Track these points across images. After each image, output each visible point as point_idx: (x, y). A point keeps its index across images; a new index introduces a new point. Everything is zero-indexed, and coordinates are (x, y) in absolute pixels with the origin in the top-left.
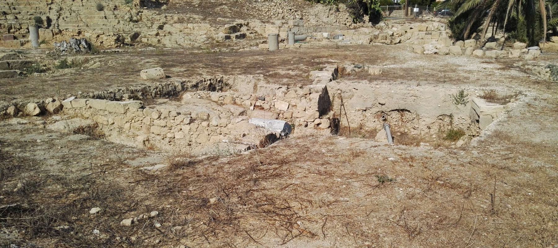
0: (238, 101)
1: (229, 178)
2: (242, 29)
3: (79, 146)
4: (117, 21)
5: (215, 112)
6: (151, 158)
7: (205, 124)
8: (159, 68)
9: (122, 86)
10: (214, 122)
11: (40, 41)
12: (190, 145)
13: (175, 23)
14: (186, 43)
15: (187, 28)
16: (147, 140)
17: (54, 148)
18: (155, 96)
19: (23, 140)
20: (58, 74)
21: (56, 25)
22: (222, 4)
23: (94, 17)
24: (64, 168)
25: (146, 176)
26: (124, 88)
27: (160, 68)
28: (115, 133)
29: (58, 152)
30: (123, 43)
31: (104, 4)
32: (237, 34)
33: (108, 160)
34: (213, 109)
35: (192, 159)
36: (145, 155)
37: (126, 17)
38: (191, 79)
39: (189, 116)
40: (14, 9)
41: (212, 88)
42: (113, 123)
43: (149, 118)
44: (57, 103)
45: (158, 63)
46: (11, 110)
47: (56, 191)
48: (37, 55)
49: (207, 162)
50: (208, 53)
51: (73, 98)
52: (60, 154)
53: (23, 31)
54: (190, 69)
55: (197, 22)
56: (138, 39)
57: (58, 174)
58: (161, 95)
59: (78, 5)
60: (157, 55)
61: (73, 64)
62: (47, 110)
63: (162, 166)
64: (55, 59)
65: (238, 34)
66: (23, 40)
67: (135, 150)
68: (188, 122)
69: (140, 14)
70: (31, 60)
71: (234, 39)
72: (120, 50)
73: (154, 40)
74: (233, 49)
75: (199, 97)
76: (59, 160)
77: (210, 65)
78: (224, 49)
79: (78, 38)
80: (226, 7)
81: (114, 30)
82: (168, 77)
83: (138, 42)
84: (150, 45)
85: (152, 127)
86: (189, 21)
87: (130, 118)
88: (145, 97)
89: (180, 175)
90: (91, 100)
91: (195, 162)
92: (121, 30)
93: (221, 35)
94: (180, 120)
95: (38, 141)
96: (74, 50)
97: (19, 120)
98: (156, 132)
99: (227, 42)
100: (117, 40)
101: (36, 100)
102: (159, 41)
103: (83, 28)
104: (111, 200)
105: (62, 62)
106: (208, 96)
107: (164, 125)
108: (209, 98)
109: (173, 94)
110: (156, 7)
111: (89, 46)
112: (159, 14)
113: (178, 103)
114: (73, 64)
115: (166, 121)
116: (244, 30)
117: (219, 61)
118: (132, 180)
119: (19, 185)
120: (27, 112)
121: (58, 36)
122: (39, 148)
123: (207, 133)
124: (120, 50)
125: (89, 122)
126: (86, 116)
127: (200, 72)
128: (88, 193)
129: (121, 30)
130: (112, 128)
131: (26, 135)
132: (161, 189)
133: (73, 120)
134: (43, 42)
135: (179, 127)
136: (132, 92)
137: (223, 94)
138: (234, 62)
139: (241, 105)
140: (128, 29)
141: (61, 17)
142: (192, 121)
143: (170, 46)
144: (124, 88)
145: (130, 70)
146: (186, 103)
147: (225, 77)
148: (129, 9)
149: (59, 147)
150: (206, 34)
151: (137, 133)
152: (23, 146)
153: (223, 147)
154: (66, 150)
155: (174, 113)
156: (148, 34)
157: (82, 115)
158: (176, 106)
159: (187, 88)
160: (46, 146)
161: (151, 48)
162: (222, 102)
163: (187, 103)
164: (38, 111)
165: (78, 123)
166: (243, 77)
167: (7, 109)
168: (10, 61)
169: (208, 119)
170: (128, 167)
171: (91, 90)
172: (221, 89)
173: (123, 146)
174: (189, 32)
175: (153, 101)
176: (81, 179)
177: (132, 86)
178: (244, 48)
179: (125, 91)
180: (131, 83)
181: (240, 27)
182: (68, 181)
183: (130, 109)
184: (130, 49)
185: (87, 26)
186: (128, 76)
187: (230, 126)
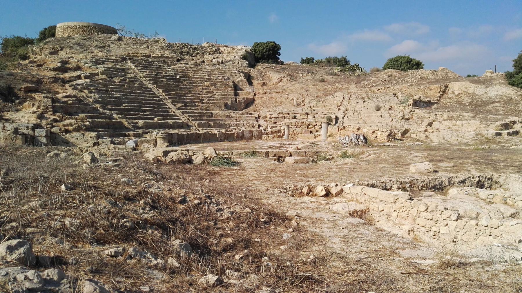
0: (509, 201)
1: (506, 288)
2: (515, 126)
3: (357, 229)
4: (391, 119)
5: (483, 210)
6: (421, 252)
7: (473, 222)
8: (427, 163)
9: (393, 178)
10: (484, 222)
11: (328, 135)
12: (455, 242)
13: (445, 120)
14: (453, 139)
15: (456, 125)
16: (412, 231)
17: (337, 228)
18: (422, 189)
19: (314, 217)
20: (341, 163)
21: (342, 122)
22: (494, 102)
23: (372, 116)
24: (345, 247)
25: (417, 269)
26: (394, 180)
27: (429, 163)
28: (383, 220)
29: (340, 232)
30: (394, 138)
31: (381, 105)
32: (509, 131)
33: (381, 247)
34: (481, 207)
35: (463, 260)
36: (415, 248)
37: (400, 115)
38: (458, 175)
39: (456, 212)
40: (314, 110)
41: (480, 185)
42: (382, 211)
43: (416, 209)
44: (339, 188)
45: (426, 157)
46: (305, 190)
47: (339, 268)
48: (325, 146)
49: (479, 266)
50: (476, 149)
51: (352, 184)
52: (342, 234)
53: (317, 127)
54: (458, 164)
55: (466, 120)
56: (408, 135)
57: (340, 252)
58: (427, 188)
59: (360, 106)
60: (425, 150)
61: (352, 155)
62: (330, 193)
63: (432, 261)
64: (338, 150)
65: (511, 131)
66: (316, 134)
67: (405, 240)
68: (455, 218)
69: (412, 113)
70: (321, 150)
71: (506, 136)
72: (391, 144)
73: (422, 136)
74: (504, 146)
75: (466, 193)
76: (341, 239)
77: (479, 162)
78: (494, 146)
79: (358, 133)
80: (499, 105)
81: (388, 127)
82: (435, 171)
83: (407, 137)
84: (418, 140)
85: (418, 219)
86: (458, 118)
87: (399, 207)
88: (412, 189)
89: (451, 275)
90: (367, 188)
91: (466, 264)
92: (394, 127)
93: (492, 131)
94: (447, 215)
95: (325, 219)
96: (354, 143)
97: (310, 198)
98: (422, 224)
99: (498, 139)
100: (390, 135)
101: (324, 184)
102: (427, 136)
103: (362, 125)
104: (385, 287)
105: (344, 153)
106: (475, 193)
107: (430, 218)
108: (476, 195)
109: (439, 188)
110: (427, 106)
111: (366, 140)
112: (430, 113)
113: (444, 197)
114: (352, 155)
115: (433, 214)
116: (517, 127)
117: (489, 158)
118: (403, 271)
119: (312, 257)
120: (316, 193)
121: (342, 131)
122: (326, 225)
123: (474, 232)
124: (391, 144)
125: (362, 207)
126: (361, 201)
127: (469, 169)
128: (365, 276)
129: (394, 127)
130: (381, 214)
131: (317, 213)
132: (432, 286)
133: (349, 203)
134: (330, 136)
135: (445, 222)
136: (401, 184)
137: (492, 192)
138: (505, 160)
139: (512, 206)
140: (399, 126)
141: (346, 116)
142: (459, 218)
143: (437, 141)
144: (394, 180)
145: (400, 163)
146: (452, 198)
147: (496, 176)
148: (402, 108)
149: (341, 228)
150: (475, 131)
151: (403, 222)
152: (315, 222)
153: (497, 251)
154: (346, 231)
155: (441, 208)
156: (417, 130)
157: (357, 200)
158: (442, 201)
159: (454, 183)
160: (330, 225)
161: (419, 143)
162: (491, 200)
163: (453, 198)
164: (324, 193)
165: (354, 206)
166: (516, 176)
167: (302, 189)
168: (307, 150)
169: (477, 216)
170: (399, 256)
171: (366, 179)
172: (490, 187)
173: (394, 235)
174: (457, 129)
175: (420, 193)
176: (359, 261)
177: (402, 178)
178: (516, 145)
179: (395, 182)
180: (401, 175)
181: (514, 124)
182: (349, 261)
183: (399, 199)
184: (400, 144)
185: (366, 123)
186: (398, 169)
187: (501, 228)
